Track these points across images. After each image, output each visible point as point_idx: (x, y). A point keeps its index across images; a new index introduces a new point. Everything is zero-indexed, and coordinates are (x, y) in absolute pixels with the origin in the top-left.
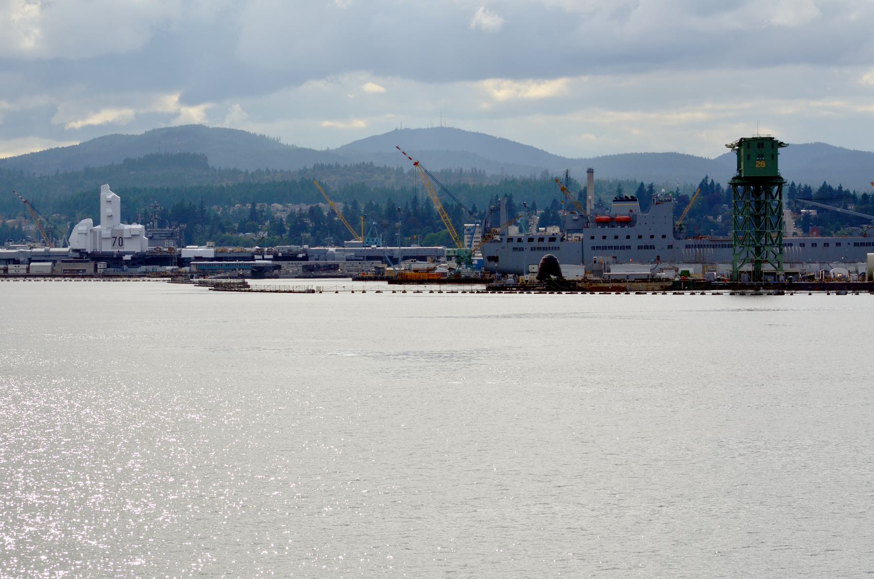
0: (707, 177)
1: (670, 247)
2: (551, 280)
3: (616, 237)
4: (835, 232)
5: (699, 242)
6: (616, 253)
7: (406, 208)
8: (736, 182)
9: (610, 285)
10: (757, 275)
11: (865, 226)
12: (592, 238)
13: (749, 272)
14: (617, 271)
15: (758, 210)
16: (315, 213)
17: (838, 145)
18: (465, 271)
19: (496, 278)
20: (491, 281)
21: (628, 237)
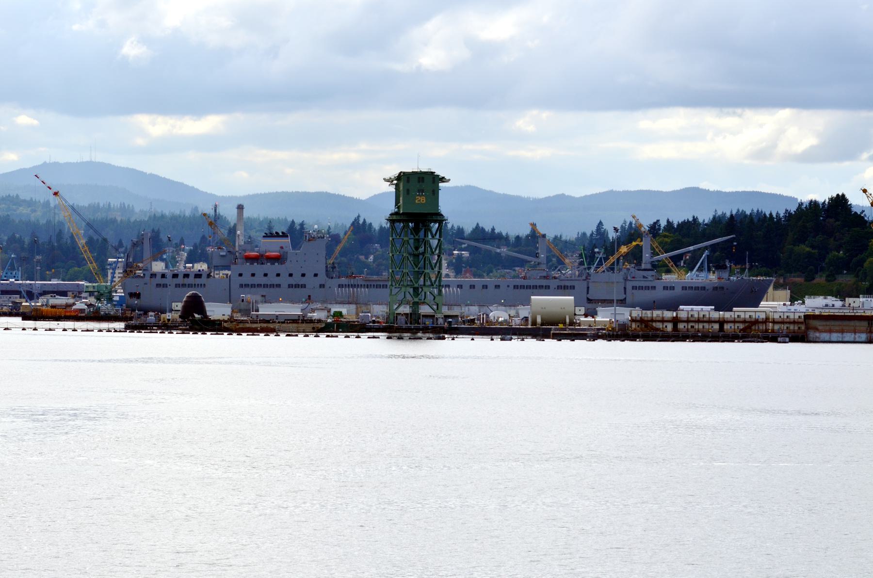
0: (359, 216)
1: (322, 286)
2: (195, 320)
3: (266, 275)
4: (488, 274)
5: (352, 282)
6: (264, 291)
7: (50, 241)
8: (394, 218)
9: (258, 326)
10: (414, 317)
11: (517, 269)
12: (241, 275)
13: (406, 314)
14: (266, 310)
15: (417, 248)
17: (488, 189)
18: (104, 307)
19: (137, 317)
20: (131, 319)
21: (278, 275)
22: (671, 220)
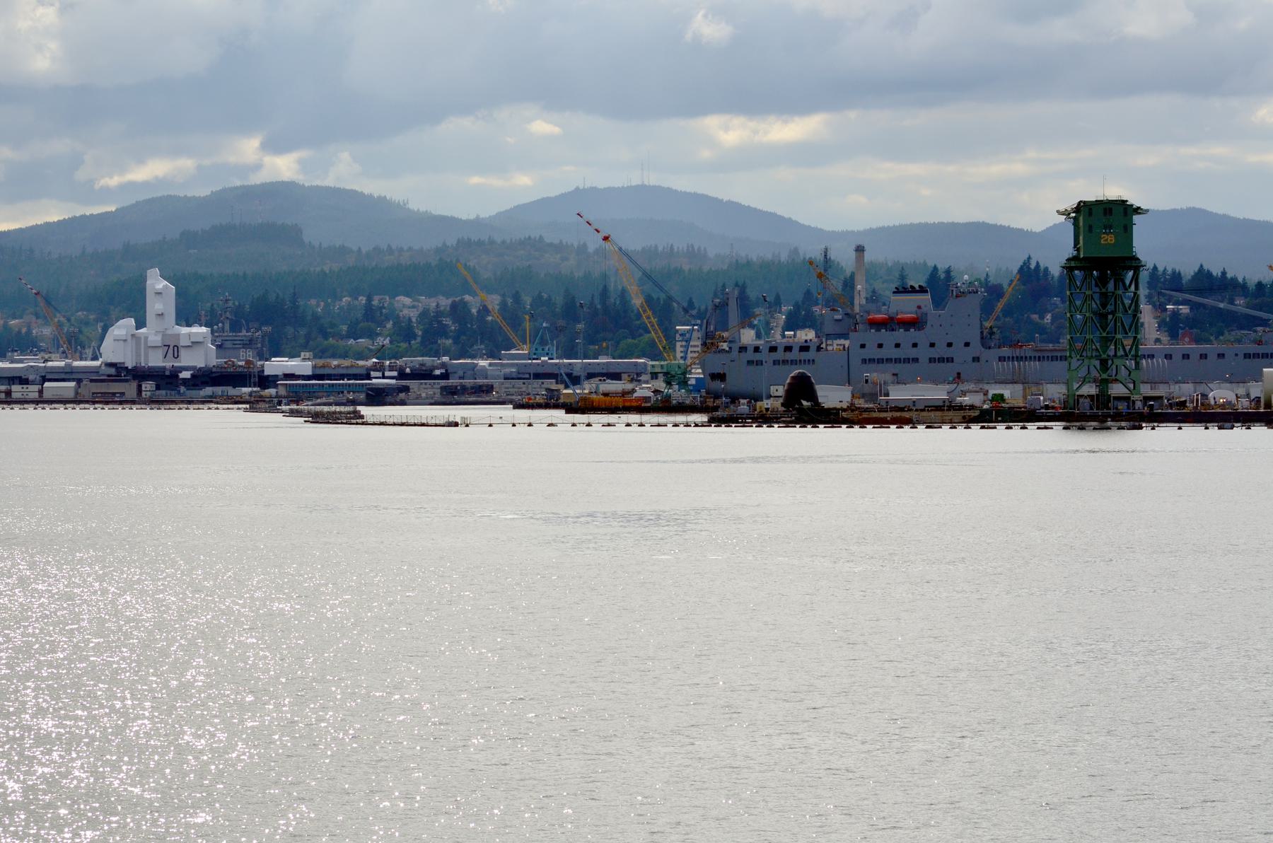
0: (1029, 258)
1: (976, 359)
2: (802, 408)
3: (897, 346)
4: (1217, 338)
5: (1018, 352)
6: (898, 368)
7: (592, 303)
8: (1073, 265)
9: (888, 415)
10: (1102, 400)
11: (1259, 329)
12: (863, 346)
13: (1091, 397)
14: (899, 394)
15: (1104, 305)
16: (458, 310)
17: (1221, 212)
18: (677, 394)
19: (722, 405)
20: (716, 409)
21: (915, 345)
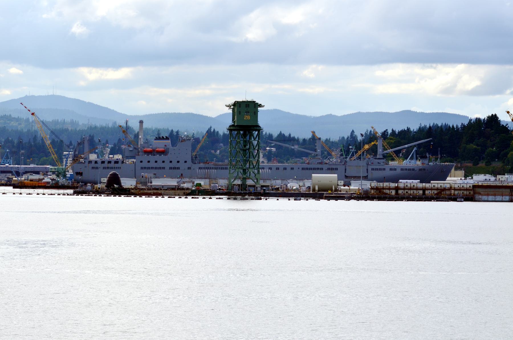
0: (211, 127)
1: (189, 168)
2: (115, 188)
3: (156, 162)
4: (287, 161)
5: (207, 166)
6: (155, 171)
7: (29, 142)
8: (232, 128)
9: (152, 191)
10: (243, 186)
11: (304, 158)
12: (141, 162)
13: (239, 185)
14: (156, 182)
15: (245, 146)
17: (287, 111)
18: (61, 180)
19: (81, 186)
20: (77, 187)
21: (163, 162)
22: (394, 130)
